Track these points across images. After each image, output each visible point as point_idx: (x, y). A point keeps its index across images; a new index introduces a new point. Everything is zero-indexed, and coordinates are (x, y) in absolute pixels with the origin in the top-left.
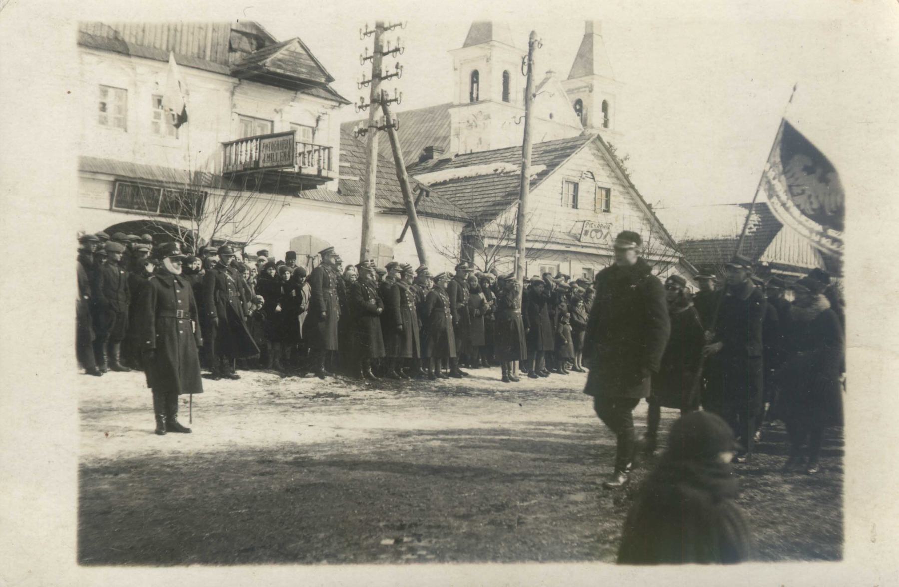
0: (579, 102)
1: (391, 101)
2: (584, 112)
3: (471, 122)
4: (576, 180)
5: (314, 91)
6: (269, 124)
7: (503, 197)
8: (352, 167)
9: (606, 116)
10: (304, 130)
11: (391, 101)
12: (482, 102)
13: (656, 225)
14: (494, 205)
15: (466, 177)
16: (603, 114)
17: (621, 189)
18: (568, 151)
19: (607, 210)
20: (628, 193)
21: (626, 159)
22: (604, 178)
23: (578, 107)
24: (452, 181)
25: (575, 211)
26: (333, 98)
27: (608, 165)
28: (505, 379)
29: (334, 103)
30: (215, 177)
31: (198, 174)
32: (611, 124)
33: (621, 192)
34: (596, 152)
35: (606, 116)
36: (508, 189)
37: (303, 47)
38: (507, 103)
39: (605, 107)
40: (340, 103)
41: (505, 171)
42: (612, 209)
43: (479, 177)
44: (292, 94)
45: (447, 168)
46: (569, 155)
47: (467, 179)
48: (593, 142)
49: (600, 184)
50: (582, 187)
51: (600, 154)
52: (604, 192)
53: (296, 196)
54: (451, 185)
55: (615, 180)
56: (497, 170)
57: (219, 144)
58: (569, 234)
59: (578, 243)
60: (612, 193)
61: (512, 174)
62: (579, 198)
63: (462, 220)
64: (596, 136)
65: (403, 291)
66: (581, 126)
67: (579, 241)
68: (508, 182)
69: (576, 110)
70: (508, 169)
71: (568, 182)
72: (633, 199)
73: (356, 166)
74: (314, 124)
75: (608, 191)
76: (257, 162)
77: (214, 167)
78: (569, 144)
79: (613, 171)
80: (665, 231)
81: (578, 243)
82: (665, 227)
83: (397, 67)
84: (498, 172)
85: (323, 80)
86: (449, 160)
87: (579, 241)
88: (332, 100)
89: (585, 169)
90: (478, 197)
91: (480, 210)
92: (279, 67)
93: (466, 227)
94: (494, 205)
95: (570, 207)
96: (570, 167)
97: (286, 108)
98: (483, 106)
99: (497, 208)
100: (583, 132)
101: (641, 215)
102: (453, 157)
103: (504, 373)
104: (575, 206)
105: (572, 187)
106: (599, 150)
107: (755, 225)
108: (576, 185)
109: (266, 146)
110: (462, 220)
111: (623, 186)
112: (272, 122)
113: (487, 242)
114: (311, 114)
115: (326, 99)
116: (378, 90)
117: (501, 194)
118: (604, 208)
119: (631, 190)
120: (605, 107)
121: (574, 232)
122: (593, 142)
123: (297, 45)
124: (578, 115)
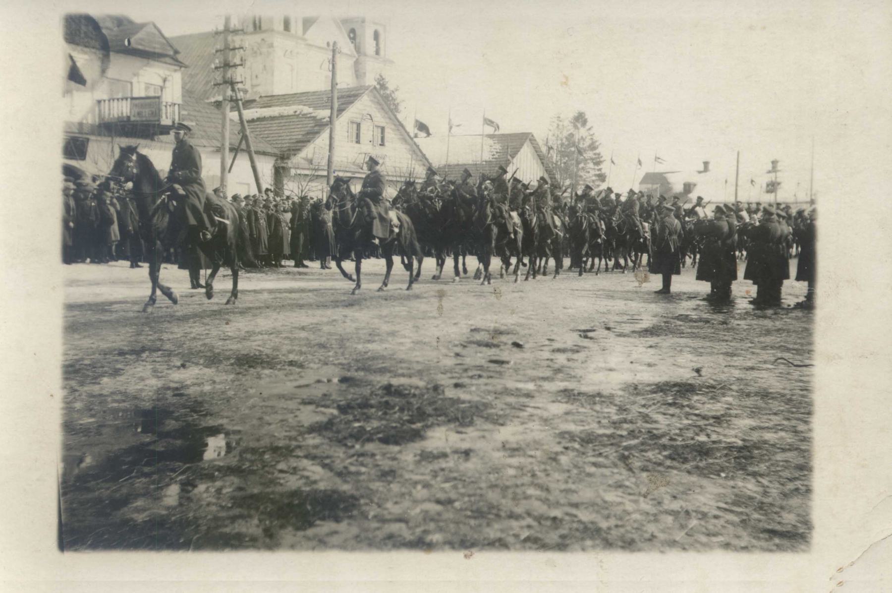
0: (353, 31)
1: (238, 83)
2: (358, 40)
3: (255, 49)
4: (358, 121)
5: (163, 59)
6: (129, 85)
7: (303, 135)
8: (189, 115)
9: (377, 44)
10: (155, 89)
11: (238, 83)
12: (265, 31)
13: (419, 154)
14: (298, 142)
15: (270, 117)
16: (375, 42)
17: (393, 127)
18: (352, 99)
19: (382, 144)
20: (398, 130)
21: (397, 90)
22: (380, 118)
23: (352, 35)
24: (259, 119)
25: (358, 145)
26: (176, 63)
27: (383, 109)
28: (322, 267)
29: (176, 68)
30: (92, 126)
31: (81, 124)
32: (382, 52)
33: (393, 130)
34: (372, 98)
35: (377, 44)
36: (307, 129)
37: (155, 27)
38: (287, 33)
39: (376, 36)
40: (181, 67)
41: (303, 113)
42: (386, 144)
43: (281, 117)
44: (145, 61)
45: (253, 108)
46: (353, 102)
47: (273, 118)
48: (371, 91)
49: (376, 123)
50: (363, 127)
51: (376, 100)
52: (380, 130)
53: (152, 139)
54: (258, 123)
55: (388, 120)
56: (296, 112)
57: (95, 101)
58: (354, 163)
59: (361, 171)
60: (387, 130)
61: (309, 116)
62: (361, 135)
63: (274, 155)
64: (372, 87)
65: (256, 213)
66: (355, 53)
67: (362, 169)
68: (305, 122)
69: (350, 38)
70: (305, 112)
71: (352, 122)
72: (402, 135)
73: (192, 113)
74: (161, 84)
75: (383, 129)
76: (129, 117)
77: (91, 120)
78: (352, 93)
79: (386, 113)
80: (427, 159)
81: (361, 171)
82: (427, 156)
83: (242, 60)
84: (297, 113)
85: (171, 53)
86: (253, 101)
87: (362, 169)
88: (175, 65)
89: (365, 113)
90: (285, 138)
91: (285, 145)
92: (141, 44)
93: (277, 160)
94: (298, 142)
95: (354, 142)
96: (353, 112)
97: (141, 72)
98: (263, 36)
99: (300, 144)
100: (357, 59)
101: (408, 147)
102: (257, 99)
103: (322, 264)
104: (358, 142)
105: (355, 126)
106: (375, 97)
107: (497, 152)
108: (359, 125)
109: (136, 105)
110: (274, 155)
111: (395, 125)
112: (131, 83)
113: (293, 172)
114: (160, 75)
115: (170, 64)
116: (229, 75)
117: (301, 133)
118: (380, 142)
119: (400, 128)
120: (376, 36)
121: (357, 161)
122: (371, 91)
123: (153, 27)
124: (352, 43)
